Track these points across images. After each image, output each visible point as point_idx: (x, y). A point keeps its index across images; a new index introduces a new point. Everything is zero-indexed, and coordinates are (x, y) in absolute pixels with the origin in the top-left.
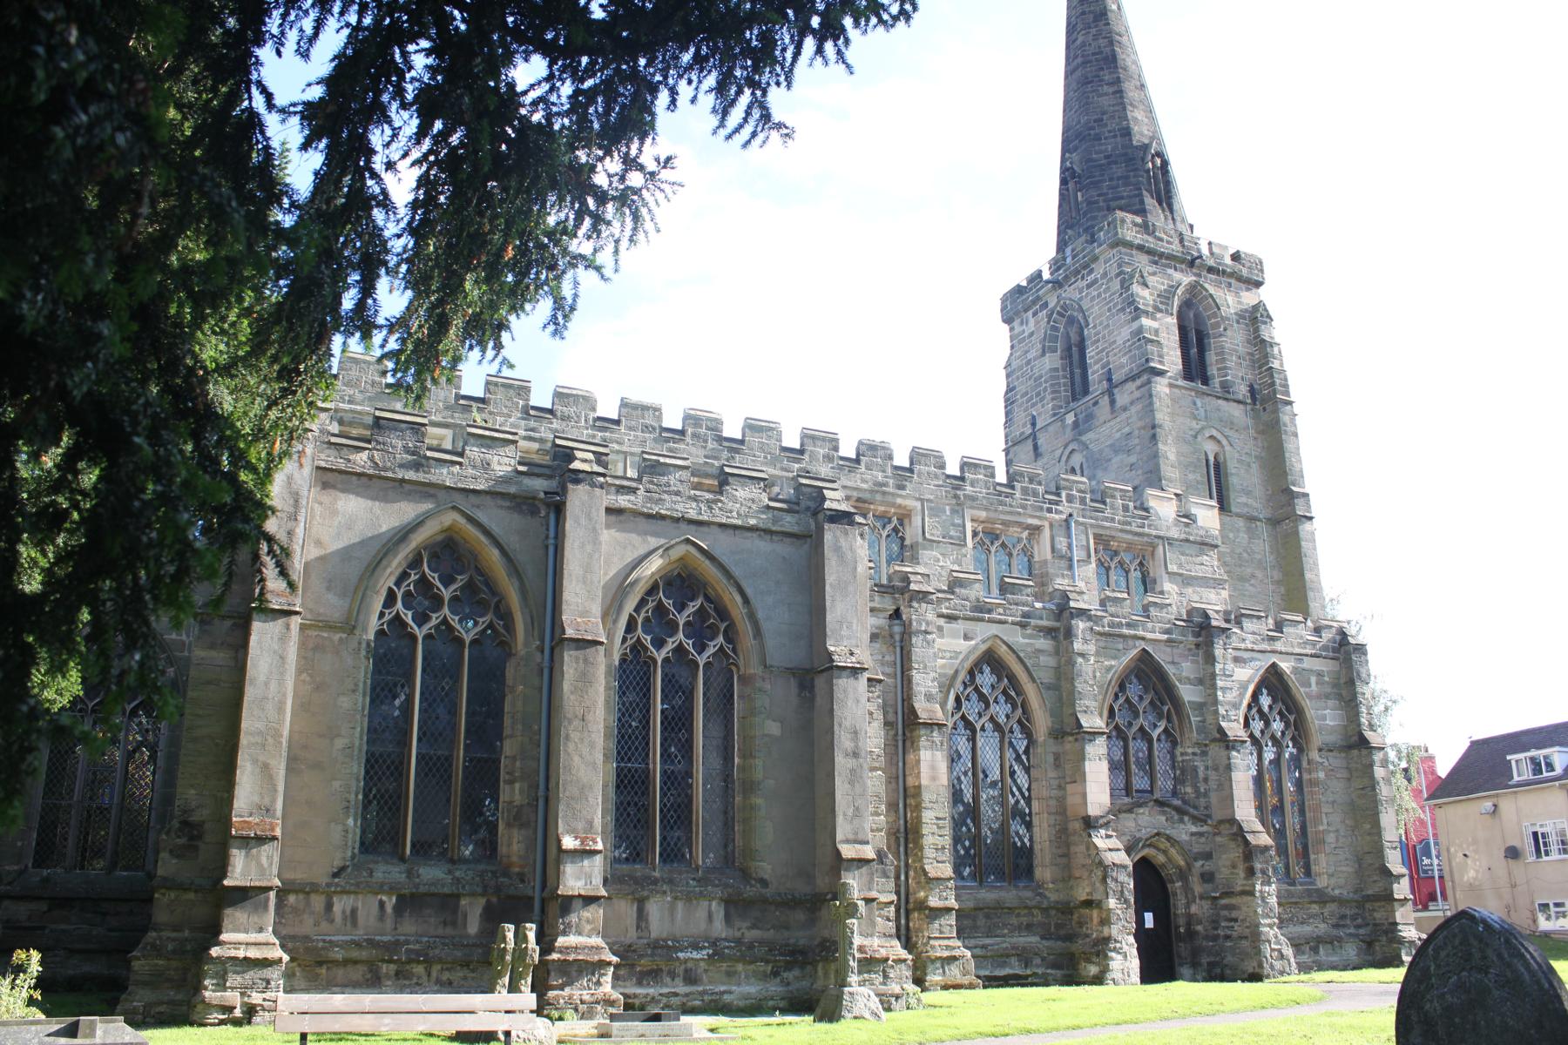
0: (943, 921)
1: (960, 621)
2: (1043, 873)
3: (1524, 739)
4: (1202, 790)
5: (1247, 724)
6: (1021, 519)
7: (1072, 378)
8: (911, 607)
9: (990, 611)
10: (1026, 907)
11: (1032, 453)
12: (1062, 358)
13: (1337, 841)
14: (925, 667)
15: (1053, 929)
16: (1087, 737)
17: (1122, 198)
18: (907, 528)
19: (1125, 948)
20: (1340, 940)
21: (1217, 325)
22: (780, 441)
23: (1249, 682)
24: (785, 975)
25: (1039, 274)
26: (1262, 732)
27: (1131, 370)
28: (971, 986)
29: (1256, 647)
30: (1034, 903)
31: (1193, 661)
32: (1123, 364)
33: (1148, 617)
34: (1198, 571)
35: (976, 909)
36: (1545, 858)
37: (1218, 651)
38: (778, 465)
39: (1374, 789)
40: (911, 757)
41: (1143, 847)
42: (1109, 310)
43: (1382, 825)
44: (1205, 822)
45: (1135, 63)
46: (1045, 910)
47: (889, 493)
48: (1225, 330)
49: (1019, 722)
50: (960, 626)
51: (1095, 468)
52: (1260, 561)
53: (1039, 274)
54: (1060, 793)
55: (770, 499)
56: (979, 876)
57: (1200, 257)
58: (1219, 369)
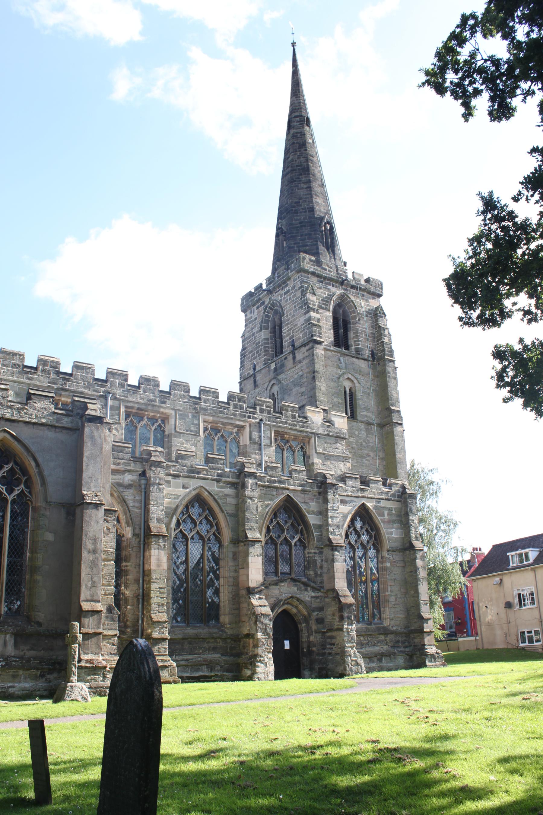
0: (160, 646)
1: (180, 478)
2: (225, 619)
3: (518, 544)
4: (319, 573)
5: (347, 536)
6: (233, 422)
7: (276, 344)
8: (151, 470)
9: (198, 473)
10: (213, 638)
11: (253, 385)
12: (271, 333)
13: (396, 600)
14: (157, 504)
15: (228, 650)
16: (250, 543)
17: (307, 246)
18: (167, 425)
19: (266, 660)
20: (394, 654)
21: (355, 317)
22: (94, 375)
23: (348, 513)
24: (48, 676)
25: (261, 286)
26: (356, 541)
27: (304, 340)
28: (175, 682)
29: (353, 494)
30: (218, 635)
31: (316, 502)
32: (300, 337)
33: (291, 477)
34: (333, 452)
35: (183, 639)
36: (524, 608)
37: (330, 496)
38: (92, 389)
39: (416, 572)
40: (147, 554)
41: (283, 604)
42: (295, 307)
43: (419, 591)
44: (320, 590)
45: (320, 172)
46: (224, 640)
47: (156, 406)
48: (359, 320)
49: (214, 534)
50: (181, 481)
51: (284, 394)
52: (372, 447)
53: (261, 286)
54: (236, 574)
55: (55, 408)
56: (187, 621)
57: (346, 280)
58: (355, 341)
